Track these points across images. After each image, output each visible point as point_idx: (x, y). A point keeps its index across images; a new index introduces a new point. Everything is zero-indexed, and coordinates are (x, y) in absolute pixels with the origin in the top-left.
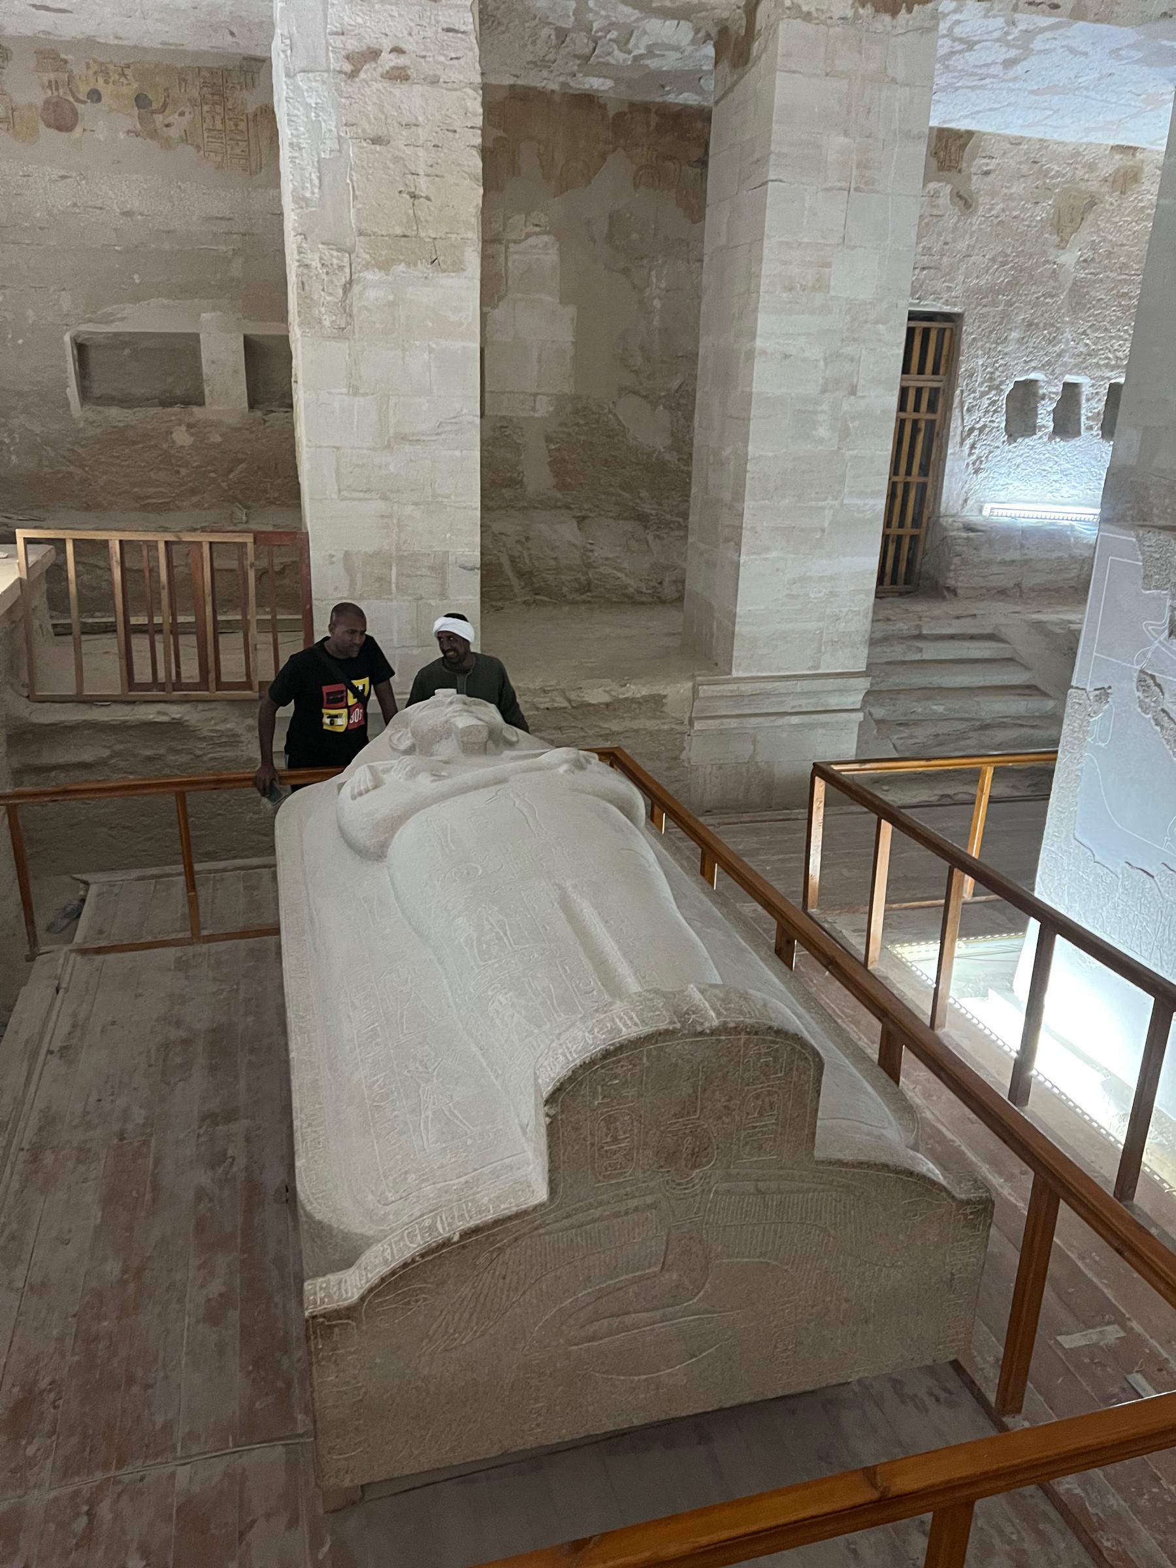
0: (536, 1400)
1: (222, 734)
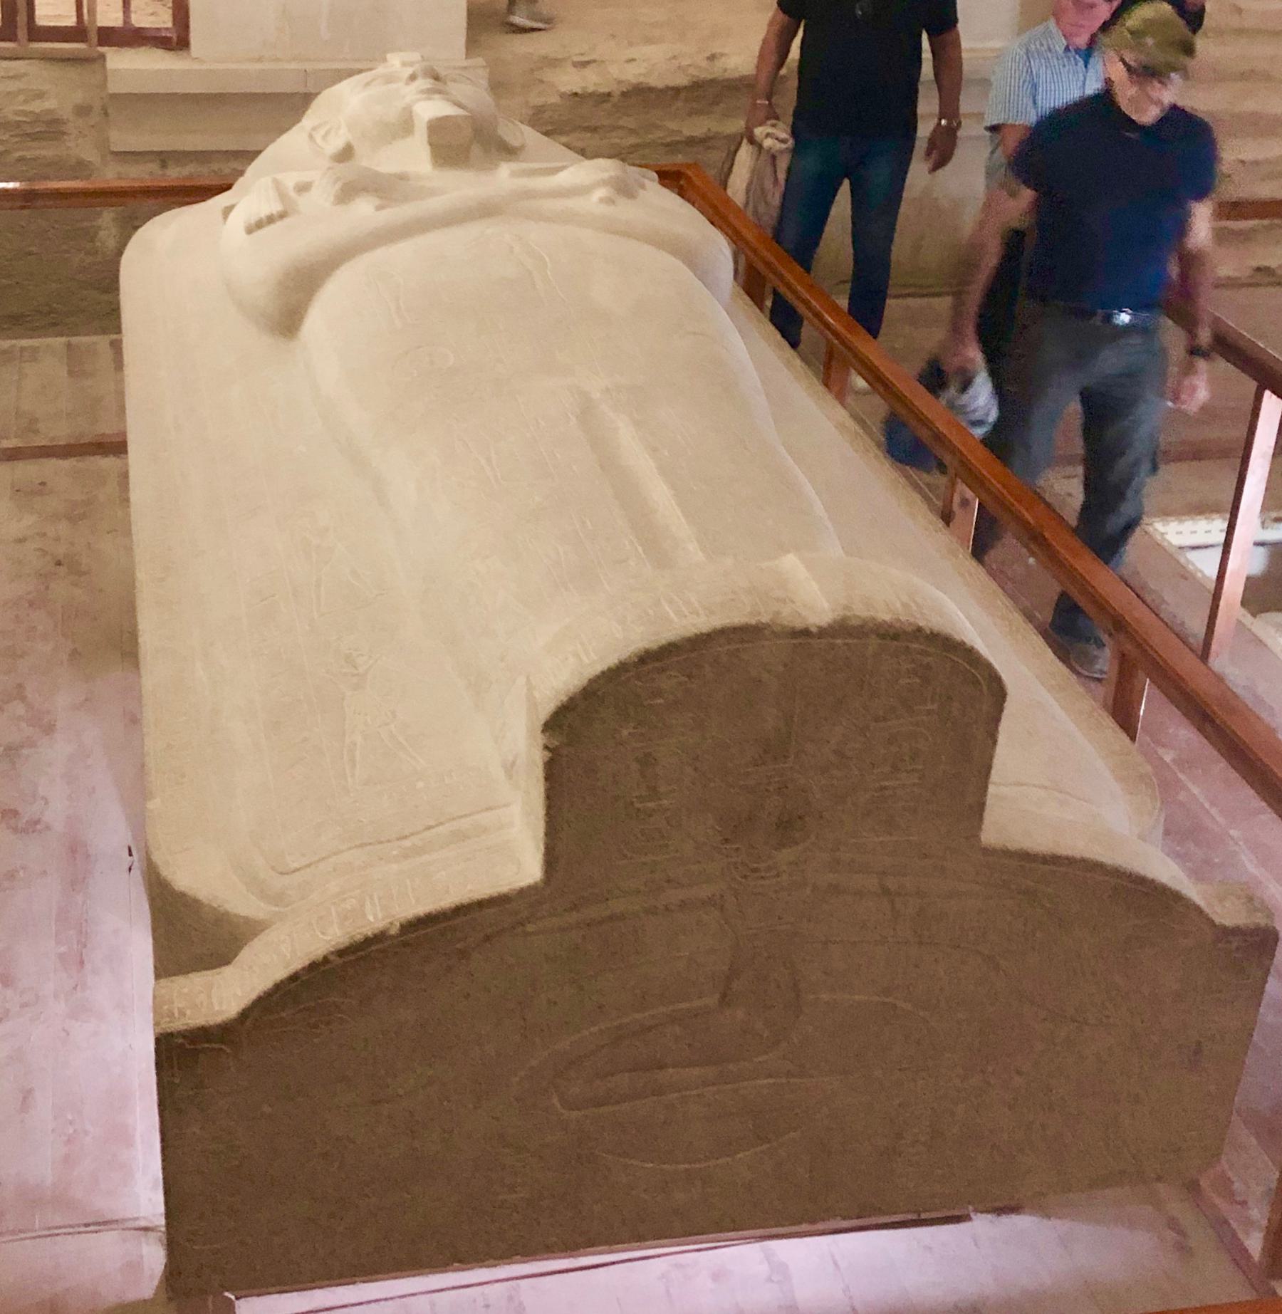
0: (512, 1189)
1: (37, 118)
